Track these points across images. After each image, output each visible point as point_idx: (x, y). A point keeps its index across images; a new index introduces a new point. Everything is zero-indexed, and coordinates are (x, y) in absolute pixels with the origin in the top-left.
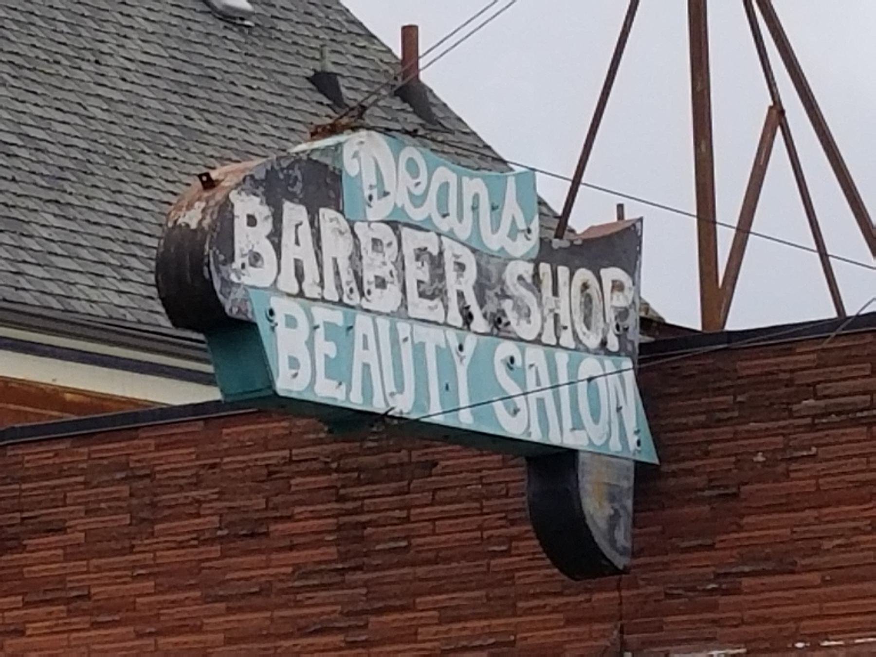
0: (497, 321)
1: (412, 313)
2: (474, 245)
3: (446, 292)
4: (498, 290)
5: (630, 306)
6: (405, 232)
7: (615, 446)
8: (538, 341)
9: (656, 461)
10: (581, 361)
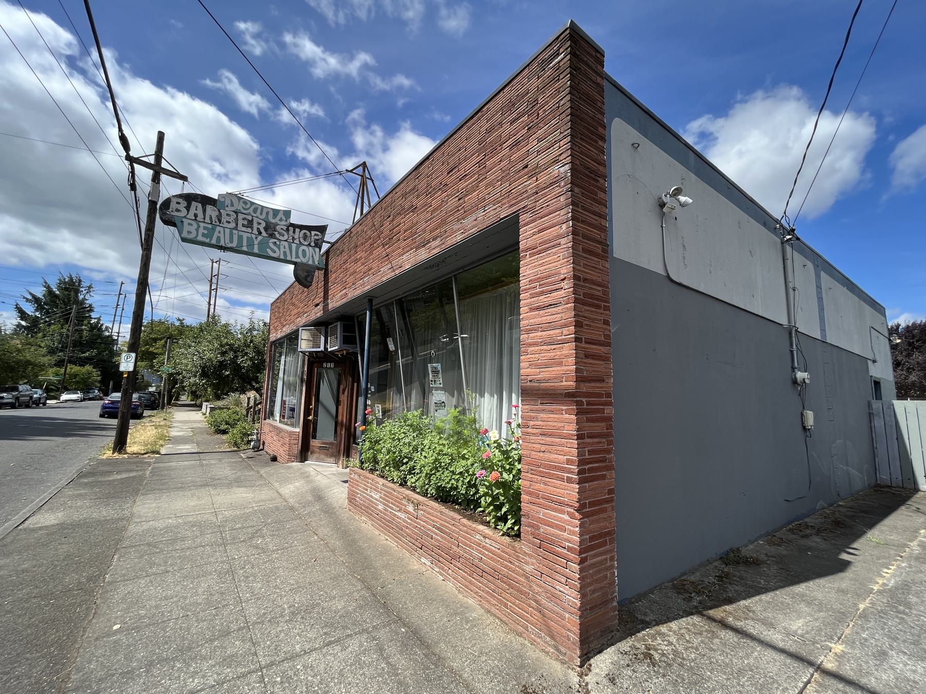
7: (310, 262)
8: (286, 241)
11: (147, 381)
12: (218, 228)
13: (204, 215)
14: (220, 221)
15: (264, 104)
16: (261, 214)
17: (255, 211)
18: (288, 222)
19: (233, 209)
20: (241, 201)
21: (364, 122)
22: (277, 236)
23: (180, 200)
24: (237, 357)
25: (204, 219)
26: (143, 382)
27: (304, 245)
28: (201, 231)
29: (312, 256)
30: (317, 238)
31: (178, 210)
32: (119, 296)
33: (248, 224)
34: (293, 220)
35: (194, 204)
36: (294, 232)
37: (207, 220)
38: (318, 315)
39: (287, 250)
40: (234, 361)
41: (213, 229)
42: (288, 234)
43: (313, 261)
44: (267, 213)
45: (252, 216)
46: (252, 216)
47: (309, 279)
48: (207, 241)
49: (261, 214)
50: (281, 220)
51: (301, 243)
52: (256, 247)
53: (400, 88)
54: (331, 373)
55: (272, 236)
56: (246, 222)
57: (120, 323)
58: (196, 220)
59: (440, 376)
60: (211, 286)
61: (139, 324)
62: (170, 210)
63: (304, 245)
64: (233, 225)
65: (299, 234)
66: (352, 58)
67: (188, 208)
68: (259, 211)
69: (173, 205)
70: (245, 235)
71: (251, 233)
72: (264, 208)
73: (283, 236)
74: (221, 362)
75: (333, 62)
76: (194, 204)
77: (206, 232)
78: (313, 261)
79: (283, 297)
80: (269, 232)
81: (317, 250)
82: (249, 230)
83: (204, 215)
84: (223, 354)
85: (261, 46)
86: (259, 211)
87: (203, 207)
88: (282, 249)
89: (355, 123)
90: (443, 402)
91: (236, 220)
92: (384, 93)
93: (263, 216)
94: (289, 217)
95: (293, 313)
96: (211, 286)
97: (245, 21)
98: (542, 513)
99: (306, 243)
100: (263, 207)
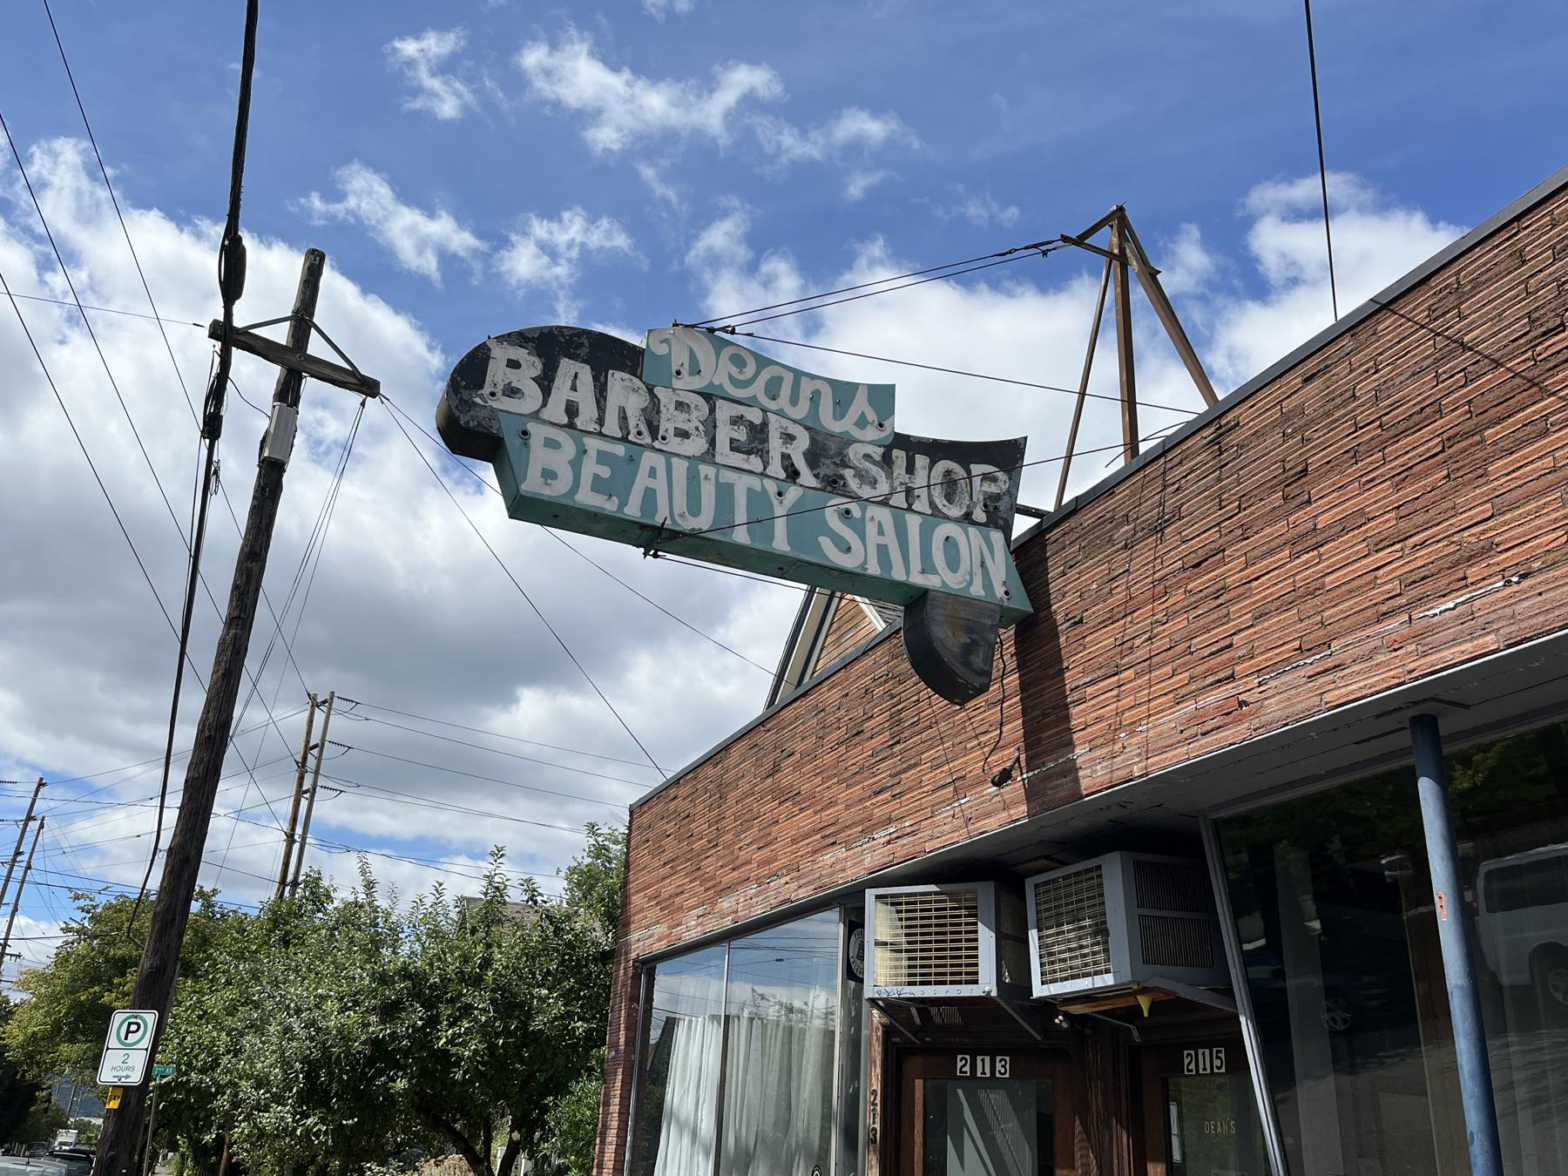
0: (834, 484)
1: (718, 459)
2: (809, 424)
3: (768, 452)
4: (838, 460)
5: (1004, 494)
6: (719, 403)
7: (977, 590)
8: (884, 503)
9: (1031, 610)
10: (938, 526)
11: (58, 1110)
12: (649, 459)
13: (601, 409)
14: (654, 430)
15: (462, 241)
16: (794, 400)
17: (773, 390)
18: (887, 432)
19: (698, 383)
20: (727, 352)
21: (743, 253)
22: (853, 484)
23: (520, 354)
24: (432, 1022)
25: (601, 421)
26: (46, 1110)
27: (947, 518)
28: (590, 468)
29: (983, 564)
30: (992, 488)
31: (512, 392)
32: (26, 825)
33: (751, 440)
34: (908, 421)
35: (567, 367)
36: (910, 469)
37: (612, 427)
38: (993, 825)
39: (890, 540)
40: (422, 1038)
41: (632, 460)
42: (890, 476)
43: (988, 584)
44: (815, 398)
45: (764, 411)
46: (764, 411)
47: (978, 660)
48: (610, 506)
49: (794, 400)
50: (862, 423)
51: (936, 513)
52: (780, 526)
53: (855, 150)
54: (996, 1100)
55: (834, 484)
56: (742, 435)
57: (15, 910)
58: (571, 425)
60: (301, 779)
61: (183, 893)
62: (486, 391)
63: (947, 518)
64: (697, 445)
65: (925, 473)
66: (709, 85)
67: (545, 383)
68: (785, 391)
69: (497, 373)
70: (742, 484)
71: (763, 475)
72: (804, 380)
73: (874, 483)
74: (376, 1043)
75: (656, 103)
76: (567, 367)
77: (605, 472)
78: (988, 584)
79: (710, 771)
80: (827, 469)
81: (997, 537)
82: (755, 463)
83: (601, 409)
84: (389, 1011)
85: (459, 95)
86: (785, 391)
87: (595, 378)
88: (873, 538)
89: (715, 261)
91: (711, 425)
92: (805, 172)
93: (801, 411)
94: (890, 411)
95: (785, 830)
96: (301, 779)
97: (417, 35)
99: (955, 512)
100: (798, 374)
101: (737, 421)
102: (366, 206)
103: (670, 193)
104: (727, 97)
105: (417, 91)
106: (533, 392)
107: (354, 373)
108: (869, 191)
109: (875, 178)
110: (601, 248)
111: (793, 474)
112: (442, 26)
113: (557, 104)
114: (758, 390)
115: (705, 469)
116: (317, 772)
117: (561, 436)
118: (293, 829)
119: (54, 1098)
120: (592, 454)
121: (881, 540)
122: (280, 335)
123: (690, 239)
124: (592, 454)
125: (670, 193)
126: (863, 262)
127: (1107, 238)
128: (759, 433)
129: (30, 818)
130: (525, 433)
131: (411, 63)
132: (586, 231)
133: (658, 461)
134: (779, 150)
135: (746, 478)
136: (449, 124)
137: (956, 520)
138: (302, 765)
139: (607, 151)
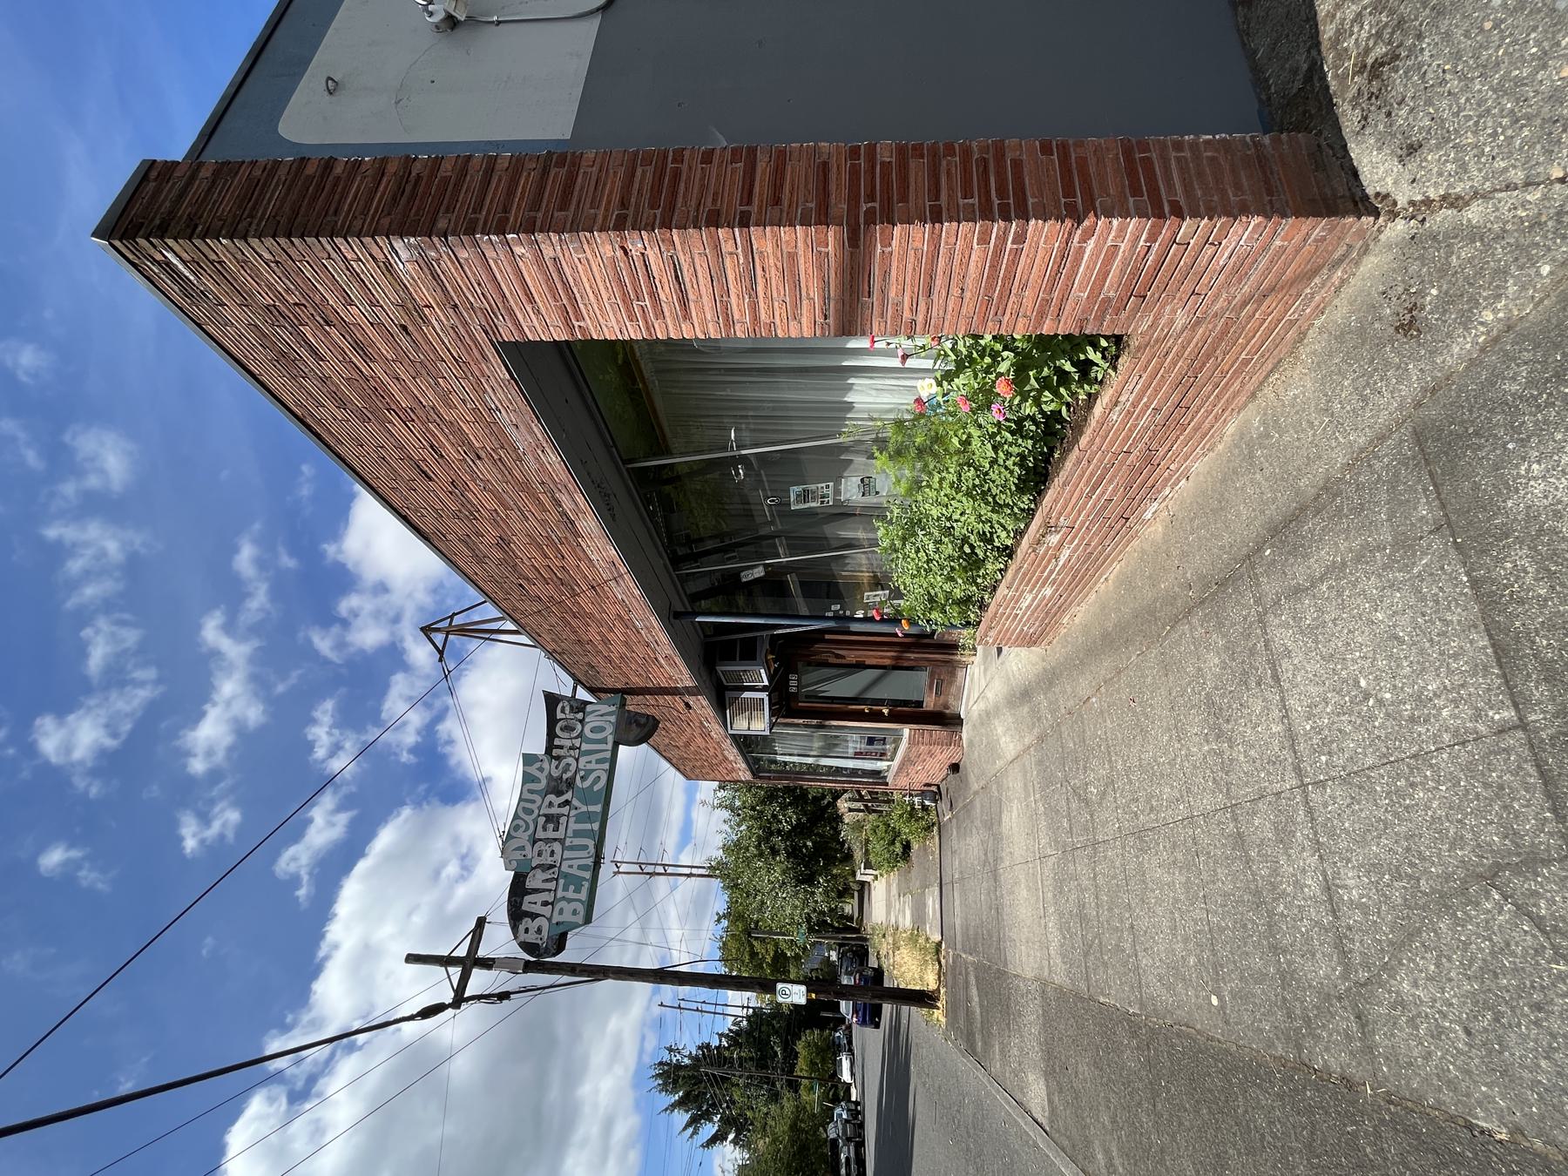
7: (613, 719)
8: (577, 760)
12: (564, 868)
13: (544, 890)
15: (327, 801)
16: (533, 802)
17: (529, 812)
19: (529, 847)
20: (513, 833)
21: (336, 629)
22: (569, 774)
23: (522, 928)
24: (779, 832)
26: (822, 970)
27: (582, 730)
28: (570, 894)
30: (567, 709)
31: (539, 931)
33: (553, 822)
34: (540, 749)
35: (525, 907)
36: (561, 747)
39: (594, 757)
40: (787, 836)
41: (566, 876)
42: (565, 757)
45: (539, 815)
46: (539, 815)
47: (643, 721)
48: (586, 885)
49: (533, 802)
50: (541, 770)
51: (580, 735)
52: (592, 808)
53: (261, 563)
55: (570, 784)
56: (551, 826)
58: (552, 904)
59: (813, 487)
61: (729, 980)
62: (540, 942)
63: (582, 730)
65: (563, 740)
66: (216, 654)
67: (534, 916)
69: (531, 938)
70: (573, 826)
71: (568, 816)
73: (568, 765)
74: (789, 855)
75: (229, 687)
76: (525, 907)
77: (572, 888)
79: (674, 761)
82: (563, 820)
83: (544, 890)
85: (222, 811)
88: (593, 766)
89: (341, 645)
90: (862, 480)
91: (547, 841)
92: (276, 593)
93: (538, 798)
97: (181, 839)
98: (1080, 293)
101: (545, 829)
102: (304, 859)
103: (295, 675)
104: (227, 645)
105: (222, 837)
106: (538, 921)
107: (474, 931)
108: (292, 554)
109: (281, 550)
110: (332, 716)
111: (567, 803)
112: (174, 825)
113: (230, 749)
114: (529, 819)
115: (568, 842)
116: (656, 864)
117: (558, 907)
118: (685, 875)
119: (816, 966)
120: (565, 894)
121: (594, 762)
122: (456, 972)
123: (326, 662)
124: (565, 894)
125: (295, 675)
126: (340, 558)
127: (439, 638)
128: (550, 818)
129: (679, 1007)
130: (557, 924)
131: (202, 842)
132: (321, 725)
133: (565, 864)
134: (260, 610)
135: (570, 825)
136: (244, 815)
137: (583, 727)
138: (651, 874)
139: (264, 712)
